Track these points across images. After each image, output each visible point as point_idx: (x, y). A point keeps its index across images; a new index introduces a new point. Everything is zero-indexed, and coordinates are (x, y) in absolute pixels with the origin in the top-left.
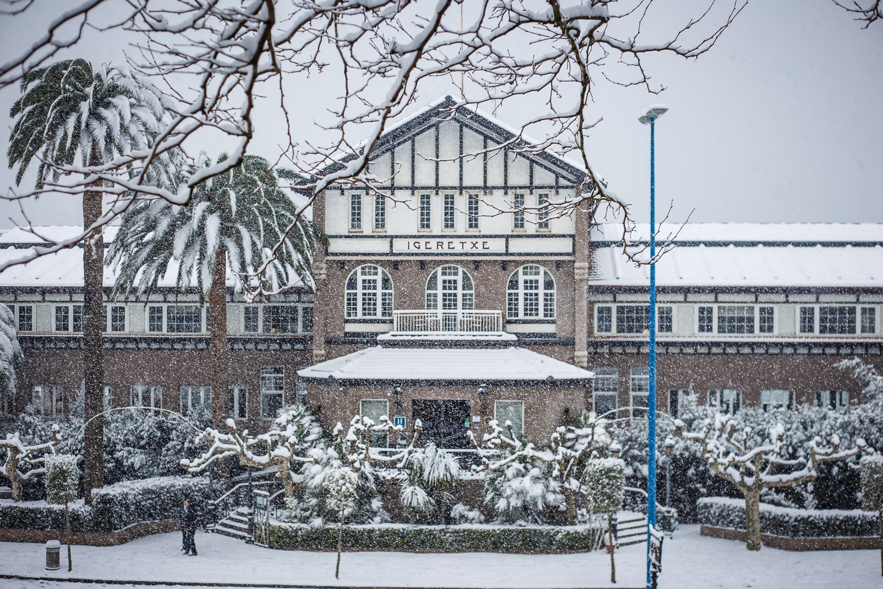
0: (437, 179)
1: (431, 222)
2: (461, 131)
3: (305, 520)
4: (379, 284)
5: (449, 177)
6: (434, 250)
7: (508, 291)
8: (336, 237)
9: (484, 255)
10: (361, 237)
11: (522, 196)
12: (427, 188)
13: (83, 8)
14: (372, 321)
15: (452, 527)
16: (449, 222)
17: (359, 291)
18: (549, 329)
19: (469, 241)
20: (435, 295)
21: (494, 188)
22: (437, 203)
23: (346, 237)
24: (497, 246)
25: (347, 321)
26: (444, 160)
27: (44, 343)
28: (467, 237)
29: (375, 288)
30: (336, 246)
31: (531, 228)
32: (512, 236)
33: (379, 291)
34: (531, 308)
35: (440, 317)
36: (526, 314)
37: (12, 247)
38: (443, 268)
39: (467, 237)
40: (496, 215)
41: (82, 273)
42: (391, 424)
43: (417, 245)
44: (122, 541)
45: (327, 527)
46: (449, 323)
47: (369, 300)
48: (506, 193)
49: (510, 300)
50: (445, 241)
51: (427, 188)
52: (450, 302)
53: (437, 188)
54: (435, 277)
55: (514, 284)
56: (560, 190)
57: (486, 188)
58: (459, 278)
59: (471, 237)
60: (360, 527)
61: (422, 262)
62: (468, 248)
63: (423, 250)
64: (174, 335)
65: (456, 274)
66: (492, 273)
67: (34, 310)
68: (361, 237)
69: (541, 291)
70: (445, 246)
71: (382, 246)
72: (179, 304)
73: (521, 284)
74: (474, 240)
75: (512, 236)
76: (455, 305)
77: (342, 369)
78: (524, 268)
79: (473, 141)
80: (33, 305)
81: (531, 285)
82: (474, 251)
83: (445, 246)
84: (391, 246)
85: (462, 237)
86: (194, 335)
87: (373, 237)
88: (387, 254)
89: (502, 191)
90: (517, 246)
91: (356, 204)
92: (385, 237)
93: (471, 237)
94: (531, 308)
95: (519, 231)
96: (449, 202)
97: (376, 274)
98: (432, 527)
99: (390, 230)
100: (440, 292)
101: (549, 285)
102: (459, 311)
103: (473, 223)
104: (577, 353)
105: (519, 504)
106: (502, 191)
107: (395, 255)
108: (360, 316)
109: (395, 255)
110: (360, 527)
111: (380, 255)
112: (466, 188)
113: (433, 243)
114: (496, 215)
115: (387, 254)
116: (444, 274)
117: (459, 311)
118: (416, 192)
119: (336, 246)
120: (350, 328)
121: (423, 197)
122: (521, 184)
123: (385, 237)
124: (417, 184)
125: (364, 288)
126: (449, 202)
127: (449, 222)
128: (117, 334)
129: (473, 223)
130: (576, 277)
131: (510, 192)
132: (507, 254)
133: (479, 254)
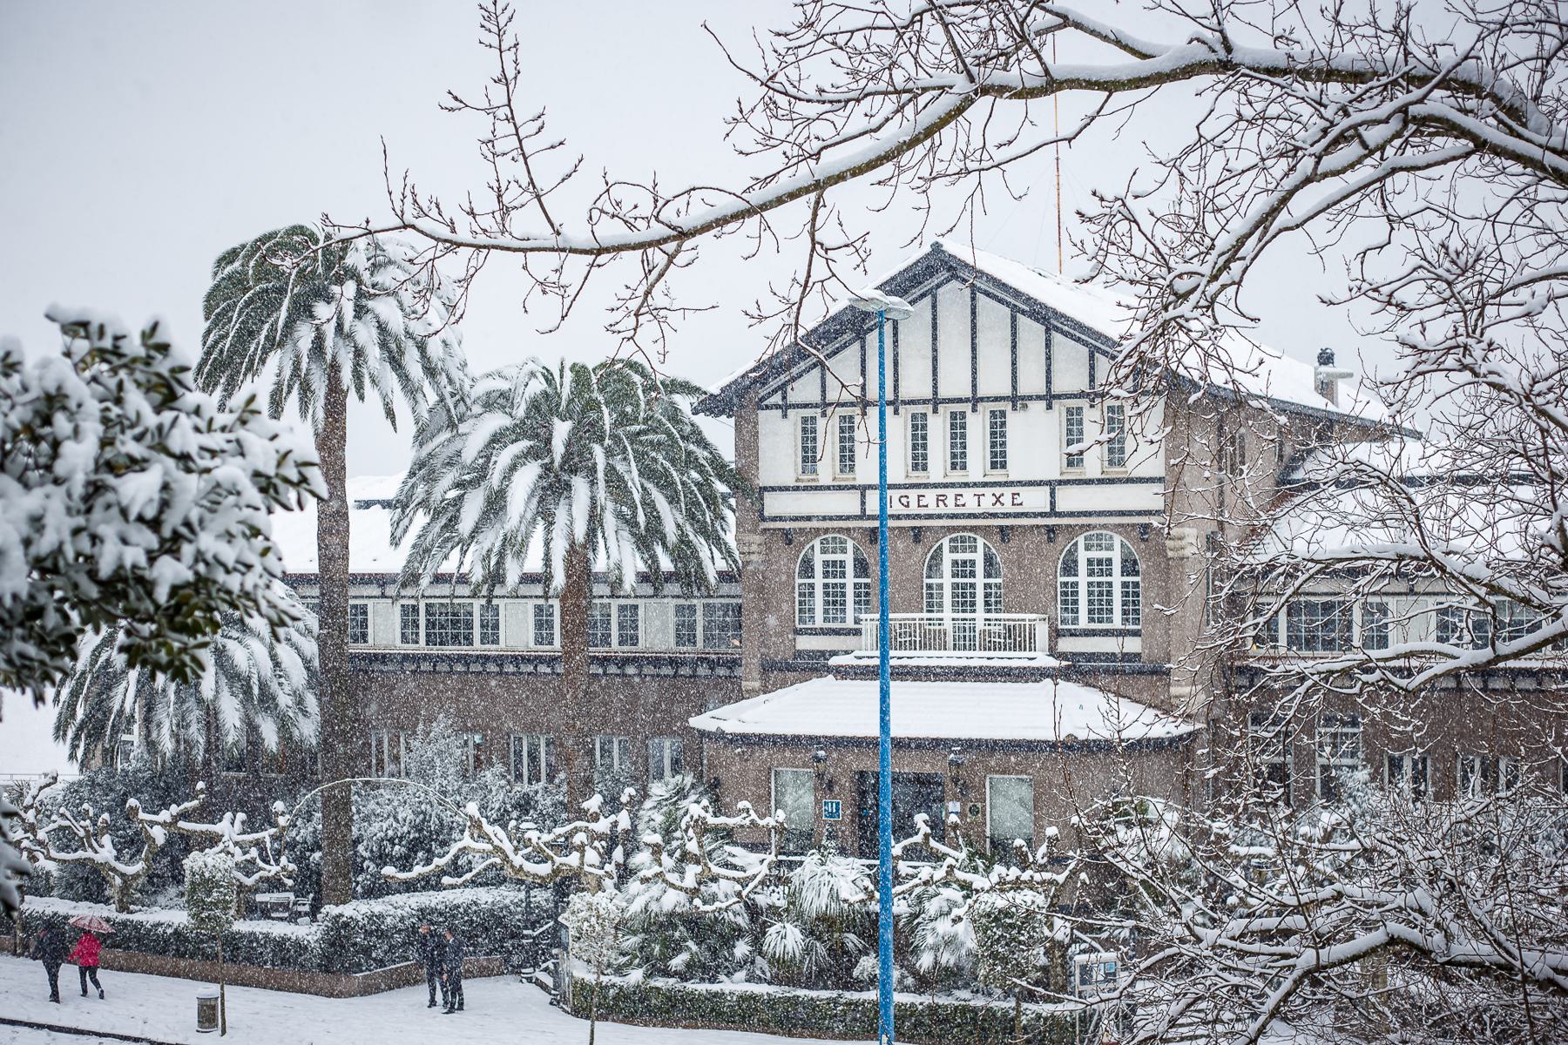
0: (935, 387)
1: (969, 460)
2: (973, 299)
3: (619, 971)
4: (980, 568)
5: (955, 383)
6: (932, 509)
7: (1061, 579)
8: (773, 489)
9: (1017, 515)
10: (817, 488)
11: (1080, 409)
12: (960, 400)
13: (1104, 77)
14: (837, 632)
15: (851, 996)
16: (958, 460)
17: (1082, 579)
18: (1133, 645)
19: (988, 491)
20: (940, 586)
21: (1030, 398)
22: (938, 427)
23: (1101, 481)
24: (1036, 500)
25: (798, 632)
26: (941, 353)
27: (640, 667)
28: (985, 485)
29: (843, 575)
30: (775, 505)
31: (1093, 465)
32: (1060, 483)
33: (980, 580)
34: (1100, 608)
35: (948, 625)
36: (1091, 620)
37: (378, 506)
38: (952, 540)
39: (985, 485)
40: (1035, 443)
41: (314, 552)
42: (754, 816)
43: (904, 500)
44: (368, 990)
45: (653, 983)
46: (965, 640)
47: (1100, 595)
48: (1049, 407)
49: (931, 596)
50: (950, 493)
51: (960, 400)
52: (964, 599)
53: (936, 402)
54: (1072, 553)
55: (1070, 568)
56: (1056, 403)
57: (1017, 400)
58: (979, 557)
59: (953, 485)
60: (703, 988)
61: (1002, 529)
62: (987, 504)
63: (914, 509)
64: (435, 650)
65: (1110, 548)
66: (1030, 546)
67: (641, 612)
68: (817, 488)
69: (1117, 579)
70: (950, 501)
71: (847, 504)
72: (456, 601)
73: (819, 569)
74: (998, 491)
75: (1060, 483)
76: (973, 604)
77: (743, 717)
78: (952, 540)
79: (993, 315)
80: (370, 603)
81: (834, 569)
82: (998, 509)
83: (950, 501)
84: (863, 503)
85: (975, 485)
86: (463, 649)
87: (797, 489)
88: (856, 518)
89: (1043, 404)
90: (1070, 499)
91: (808, 432)
92: (853, 487)
93: (953, 485)
94: (1100, 608)
95: (1074, 473)
96: (958, 426)
97: (844, 551)
98: (814, 994)
99: (1015, 472)
100: (947, 580)
101: (1130, 567)
102: (980, 614)
103: (998, 460)
104: (1174, 690)
105: (952, 962)
106: (1043, 404)
107: (1060, 515)
108: (819, 622)
109: (1060, 515)
110: (703, 988)
111: (1035, 515)
112: (1059, 397)
113: (930, 496)
114: (1035, 443)
115: (856, 518)
116: (954, 550)
117: (980, 614)
118: (829, 410)
119: (775, 505)
120: (805, 643)
121: (805, 420)
122: (1075, 389)
123: (853, 487)
124: (942, 394)
125: (826, 575)
126: (958, 426)
127: (958, 460)
128: (491, 650)
129: (998, 460)
130: (1170, 554)
131: (980, 406)
132: (1053, 513)
133: (1007, 515)
